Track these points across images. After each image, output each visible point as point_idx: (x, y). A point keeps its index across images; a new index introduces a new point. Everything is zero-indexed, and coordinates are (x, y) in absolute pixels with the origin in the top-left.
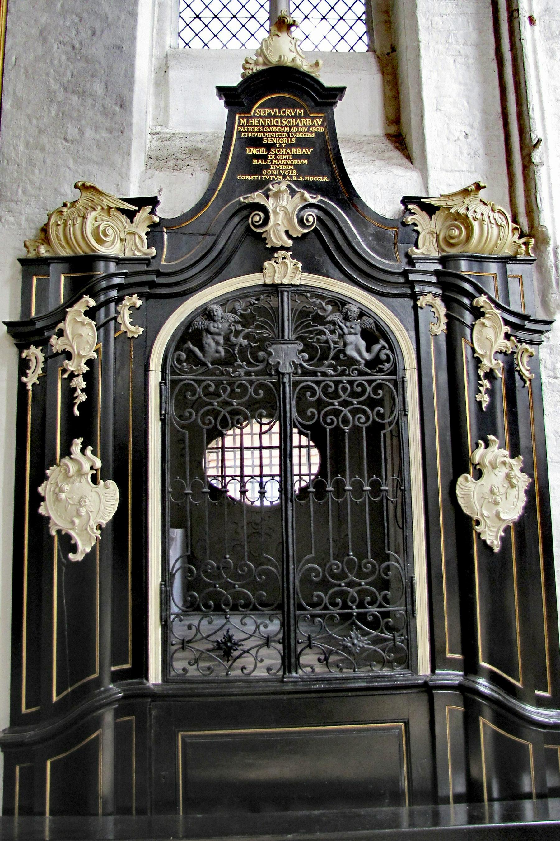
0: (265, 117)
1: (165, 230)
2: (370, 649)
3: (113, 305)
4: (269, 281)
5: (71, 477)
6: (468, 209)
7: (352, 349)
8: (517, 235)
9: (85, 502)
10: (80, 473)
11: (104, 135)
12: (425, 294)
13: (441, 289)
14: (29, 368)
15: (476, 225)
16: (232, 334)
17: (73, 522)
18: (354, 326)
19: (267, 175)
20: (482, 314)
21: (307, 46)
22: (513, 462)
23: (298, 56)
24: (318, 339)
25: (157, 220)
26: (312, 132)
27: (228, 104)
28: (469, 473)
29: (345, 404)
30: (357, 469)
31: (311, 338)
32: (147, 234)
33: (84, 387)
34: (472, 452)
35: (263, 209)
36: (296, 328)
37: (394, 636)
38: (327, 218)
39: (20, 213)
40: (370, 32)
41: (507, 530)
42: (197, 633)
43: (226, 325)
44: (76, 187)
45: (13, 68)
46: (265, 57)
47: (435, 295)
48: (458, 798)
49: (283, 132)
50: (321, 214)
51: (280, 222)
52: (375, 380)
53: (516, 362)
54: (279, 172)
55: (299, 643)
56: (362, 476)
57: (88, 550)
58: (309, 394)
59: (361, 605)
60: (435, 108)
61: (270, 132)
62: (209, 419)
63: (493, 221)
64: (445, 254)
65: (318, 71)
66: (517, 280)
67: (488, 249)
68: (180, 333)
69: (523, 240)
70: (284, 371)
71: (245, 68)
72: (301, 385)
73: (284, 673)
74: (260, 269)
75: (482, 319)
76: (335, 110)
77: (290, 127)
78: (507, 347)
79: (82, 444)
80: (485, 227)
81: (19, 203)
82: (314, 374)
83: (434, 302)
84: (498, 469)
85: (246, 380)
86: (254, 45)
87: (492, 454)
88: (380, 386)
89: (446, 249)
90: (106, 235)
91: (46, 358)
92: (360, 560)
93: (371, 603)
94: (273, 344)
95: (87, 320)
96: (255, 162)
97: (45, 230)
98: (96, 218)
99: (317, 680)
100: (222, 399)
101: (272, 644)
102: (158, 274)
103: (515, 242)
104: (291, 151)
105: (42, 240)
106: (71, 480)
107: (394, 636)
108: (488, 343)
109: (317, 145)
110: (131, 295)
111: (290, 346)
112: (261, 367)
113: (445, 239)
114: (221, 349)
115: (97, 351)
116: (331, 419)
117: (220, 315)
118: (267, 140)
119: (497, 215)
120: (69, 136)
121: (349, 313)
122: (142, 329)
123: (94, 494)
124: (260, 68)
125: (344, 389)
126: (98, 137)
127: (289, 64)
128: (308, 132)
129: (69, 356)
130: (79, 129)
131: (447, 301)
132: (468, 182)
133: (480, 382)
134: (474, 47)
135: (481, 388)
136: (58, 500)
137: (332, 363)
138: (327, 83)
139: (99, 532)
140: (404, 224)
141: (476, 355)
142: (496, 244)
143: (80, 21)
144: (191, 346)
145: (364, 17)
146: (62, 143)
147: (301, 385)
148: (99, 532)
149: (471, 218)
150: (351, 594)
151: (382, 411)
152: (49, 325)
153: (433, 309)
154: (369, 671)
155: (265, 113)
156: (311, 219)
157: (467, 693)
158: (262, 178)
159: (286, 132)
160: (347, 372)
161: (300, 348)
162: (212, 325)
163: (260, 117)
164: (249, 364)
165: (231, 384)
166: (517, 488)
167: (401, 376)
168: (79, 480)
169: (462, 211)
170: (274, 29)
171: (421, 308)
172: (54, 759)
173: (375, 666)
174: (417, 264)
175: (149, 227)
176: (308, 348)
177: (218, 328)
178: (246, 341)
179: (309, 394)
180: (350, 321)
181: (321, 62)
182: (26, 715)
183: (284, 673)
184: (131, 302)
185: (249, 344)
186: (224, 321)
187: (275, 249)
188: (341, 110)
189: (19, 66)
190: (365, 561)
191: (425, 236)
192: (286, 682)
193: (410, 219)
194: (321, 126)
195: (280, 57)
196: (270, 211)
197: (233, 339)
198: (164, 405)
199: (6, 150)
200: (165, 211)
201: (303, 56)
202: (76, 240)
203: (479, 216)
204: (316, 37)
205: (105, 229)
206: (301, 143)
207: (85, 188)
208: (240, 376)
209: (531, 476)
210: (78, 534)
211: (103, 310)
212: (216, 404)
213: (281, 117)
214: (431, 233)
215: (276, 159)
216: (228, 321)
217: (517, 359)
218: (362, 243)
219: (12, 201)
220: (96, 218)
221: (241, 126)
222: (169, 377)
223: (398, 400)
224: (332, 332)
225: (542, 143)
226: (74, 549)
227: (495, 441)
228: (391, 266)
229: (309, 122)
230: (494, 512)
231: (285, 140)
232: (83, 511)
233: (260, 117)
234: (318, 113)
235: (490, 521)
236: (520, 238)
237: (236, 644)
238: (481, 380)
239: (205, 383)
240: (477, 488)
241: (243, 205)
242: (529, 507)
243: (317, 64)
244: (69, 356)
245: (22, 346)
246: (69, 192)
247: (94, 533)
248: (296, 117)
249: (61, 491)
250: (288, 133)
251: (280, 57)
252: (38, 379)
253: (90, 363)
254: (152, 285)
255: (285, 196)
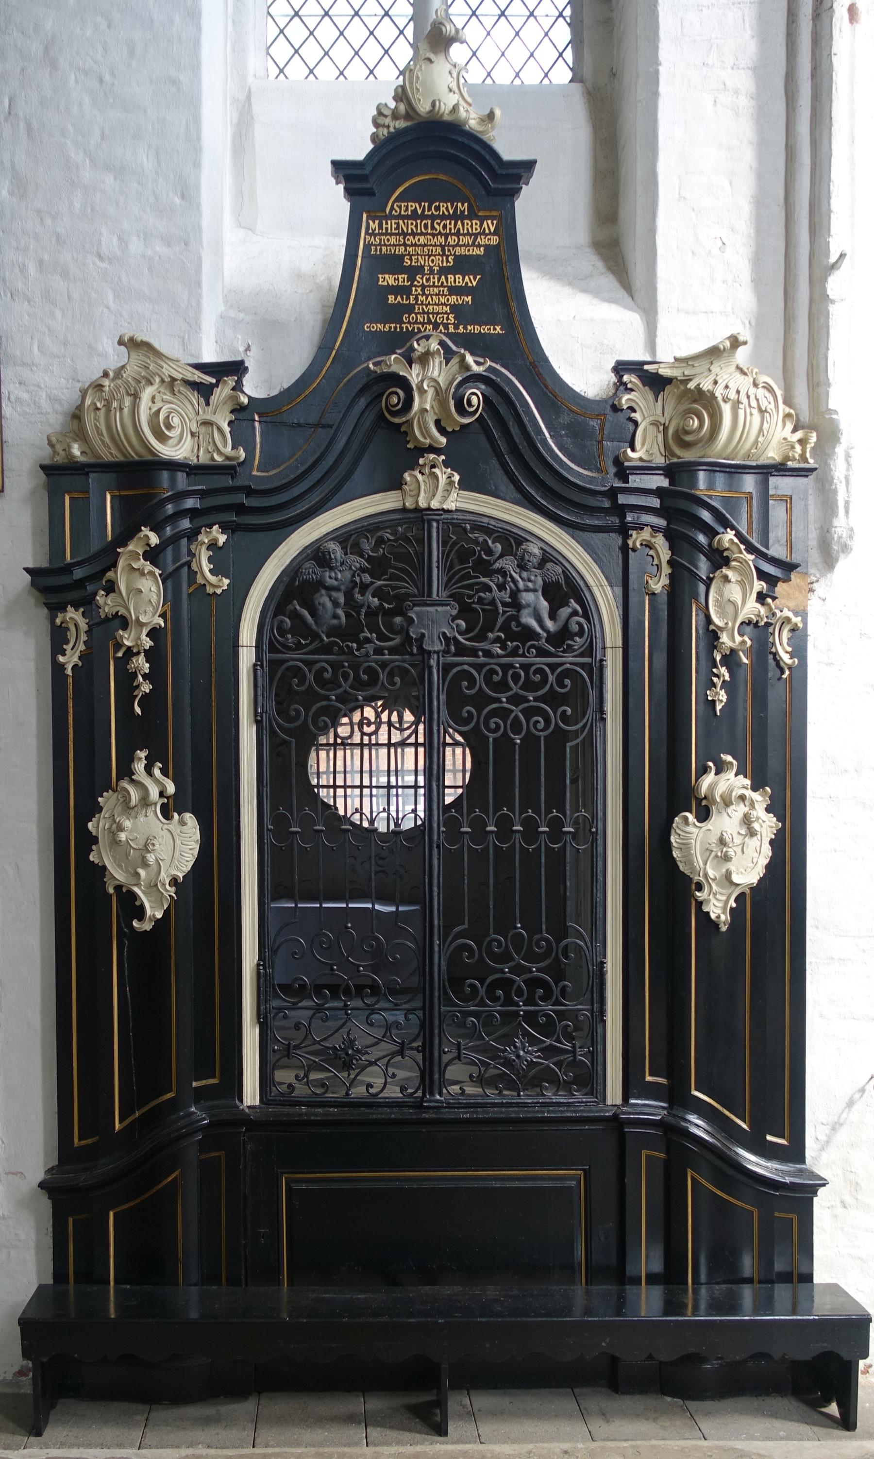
0: (407, 217)
1: (257, 418)
2: (543, 1064)
3: (184, 541)
4: (409, 504)
5: (133, 808)
6: (716, 382)
7: (529, 615)
8: (790, 426)
9: (153, 845)
10: (145, 801)
11: (158, 249)
12: (640, 527)
13: (666, 519)
14: (67, 642)
15: (726, 410)
16: (357, 590)
17: (137, 875)
18: (533, 578)
19: (409, 322)
20: (726, 562)
21: (475, 75)
22: (756, 796)
23: (462, 102)
24: (480, 598)
25: (245, 400)
26: (479, 246)
27: (350, 193)
28: (691, 812)
29: (516, 700)
30: (530, 800)
31: (470, 597)
32: (230, 423)
33: (147, 671)
34: (697, 780)
35: (404, 384)
36: (449, 581)
37: (574, 1046)
38: (500, 400)
39: (39, 386)
40: (576, 42)
41: (740, 898)
42: (307, 1035)
43: (348, 575)
44: (121, 342)
45: (6, 120)
46: (409, 104)
47: (655, 529)
48: (652, 1279)
49: (435, 245)
50: (489, 391)
51: (428, 407)
52: (562, 664)
53: (771, 640)
54: (428, 318)
55: (445, 1053)
56: (537, 811)
57: (159, 915)
58: (465, 683)
59: (529, 1002)
60: (677, 196)
61: (416, 245)
62: (324, 721)
63: (754, 403)
64: (675, 460)
65: (493, 128)
66: (784, 504)
67: (742, 452)
68: (282, 587)
69: (799, 435)
70: (431, 649)
71: (376, 124)
72: (455, 670)
73: (424, 1095)
74: (397, 484)
75: (725, 571)
76: (518, 204)
77: (446, 236)
78: (759, 616)
79: (146, 758)
80: (741, 413)
81: (34, 368)
82: (473, 652)
83: (653, 540)
84: (732, 807)
85: (376, 662)
86: (389, 77)
87: (726, 782)
88: (566, 674)
89: (677, 451)
90: (169, 427)
91: (91, 627)
92: (530, 937)
93: (544, 998)
94: (414, 605)
95: (148, 567)
96: (391, 299)
97: (77, 416)
98: (153, 398)
99: (468, 1106)
100: (342, 690)
101: (407, 1052)
102: (249, 491)
103: (785, 439)
104: (447, 279)
105: (75, 433)
106: (133, 813)
107: (574, 1046)
108: (730, 610)
109: (488, 269)
110: (210, 526)
111: (439, 609)
112: (397, 640)
113: (676, 434)
114: (340, 612)
115: (163, 615)
116: (495, 723)
117: (339, 558)
118: (411, 260)
119: (761, 393)
120: (104, 250)
121: (527, 557)
122: (226, 581)
123: (166, 833)
124: (401, 124)
125: (516, 677)
126: (149, 252)
127: (446, 118)
128: (473, 245)
129: (124, 623)
130: (119, 238)
131: (670, 536)
132: (718, 336)
133: (715, 670)
134: (750, 72)
135: (715, 679)
136: (115, 842)
137: (499, 637)
138: (507, 155)
139: (173, 889)
140: (616, 409)
141: (712, 627)
142: (756, 441)
143: (109, 27)
144: (298, 607)
145: (568, 12)
146: (94, 264)
147: (455, 670)
148: (173, 889)
149: (720, 399)
150: (517, 983)
151: (569, 711)
152: (96, 573)
153: (652, 553)
154: (538, 1095)
155: (407, 210)
156: (474, 400)
157: (673, 1134)
158: (401, 328)
159: (441, 245)
160: (521, 652)
161: (454, 612)
162: (327, 574)
163: (400, 217)
164: (382, 637)
165: (355, 667)
166: (759, 836)
167: (598, 659)
168: (144, 812)
169: (706, 385)
170: (423, 46)
171: (634, 550)
172: (118, 1209)
173: (546, 1088)
174: (631, 478)
175: (232, 412)
176: (466, 611)
177: (336, 579)
178: (376, 599)
179: (465, 683)
180: (527, 570)
181: (498, 112)
182: (80, 1148)
183: (424, 1095)
184: (211, 537)
185: (381, 605)
186: (345, 569)
187: (422, 451)
188: (528, 206)
189: (16, 115)
190: (537, 937)
191: (645, 429)
192: (426, 1107)
193: (625, 400)
194: (494, 234)
195: (433, 104)
196: (414, 387)
197: (358, 597)
198: (260, 699)
199: (7, 274)
200: (254, 387)
201: (469, 100)
202: (126, 435)
203: (733, 395)
204: (489, 54)
205: (168, 417)
206: (463, 265)
207: (133, 344)
208: (367, 655)
209: (781, 818)
210: (144, 892)
211: (169, 551)
212: (334, 697)
213: (433, 218)
214: (655, 424)
215: (424, 294)
216: (351, 568)
217: (773, 634)
218: (550, 441)
219: (24, 364)
220: (153, 398)
221: (371, 235)
222: (267, 656)
223: (592, 696)
224: (501, 587)
225: (847, 260)
226: (140, 912)
227: (731, 763)
228: (591, 480)
229: (474, 226)
230: (724, 870)
231: (438, 260)
232: (151, 858)
233: (400, 217)
234: (490, 210)
235: (717, 885)
236: (795, 430)
237: (358, 1051)
238: (716, 667)
239: (318, 666)
240: (701, 835)
241: (373, 375)
242: (774, 868)
243: (491, 116)
244: (124, 623)
245: (55, 608)
246: (110, 350)
247: (167, 891)
248: (456, 217)
249: (120, 829)
250: (443, 247)
251: (433, 104)
252: (80, 658)
253: (154, 633)
254: (240, 509)
255: (437, 361)
